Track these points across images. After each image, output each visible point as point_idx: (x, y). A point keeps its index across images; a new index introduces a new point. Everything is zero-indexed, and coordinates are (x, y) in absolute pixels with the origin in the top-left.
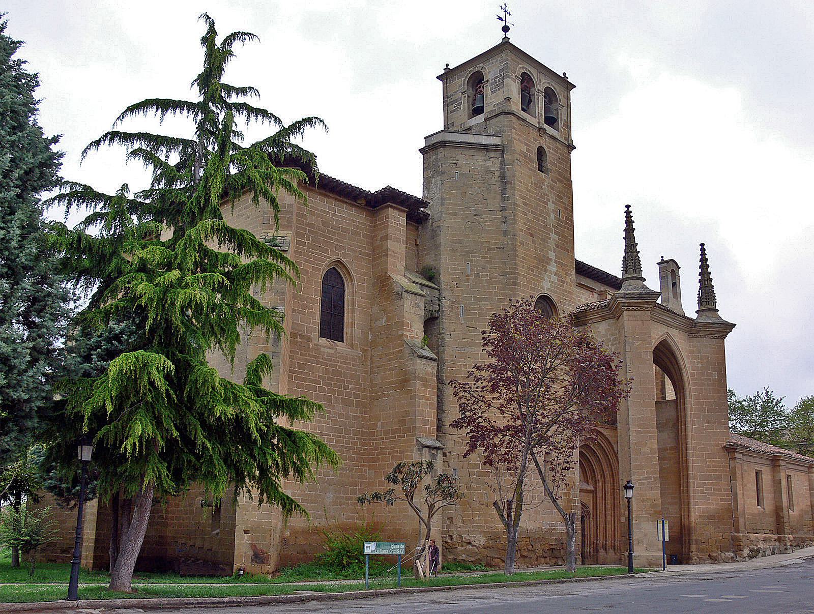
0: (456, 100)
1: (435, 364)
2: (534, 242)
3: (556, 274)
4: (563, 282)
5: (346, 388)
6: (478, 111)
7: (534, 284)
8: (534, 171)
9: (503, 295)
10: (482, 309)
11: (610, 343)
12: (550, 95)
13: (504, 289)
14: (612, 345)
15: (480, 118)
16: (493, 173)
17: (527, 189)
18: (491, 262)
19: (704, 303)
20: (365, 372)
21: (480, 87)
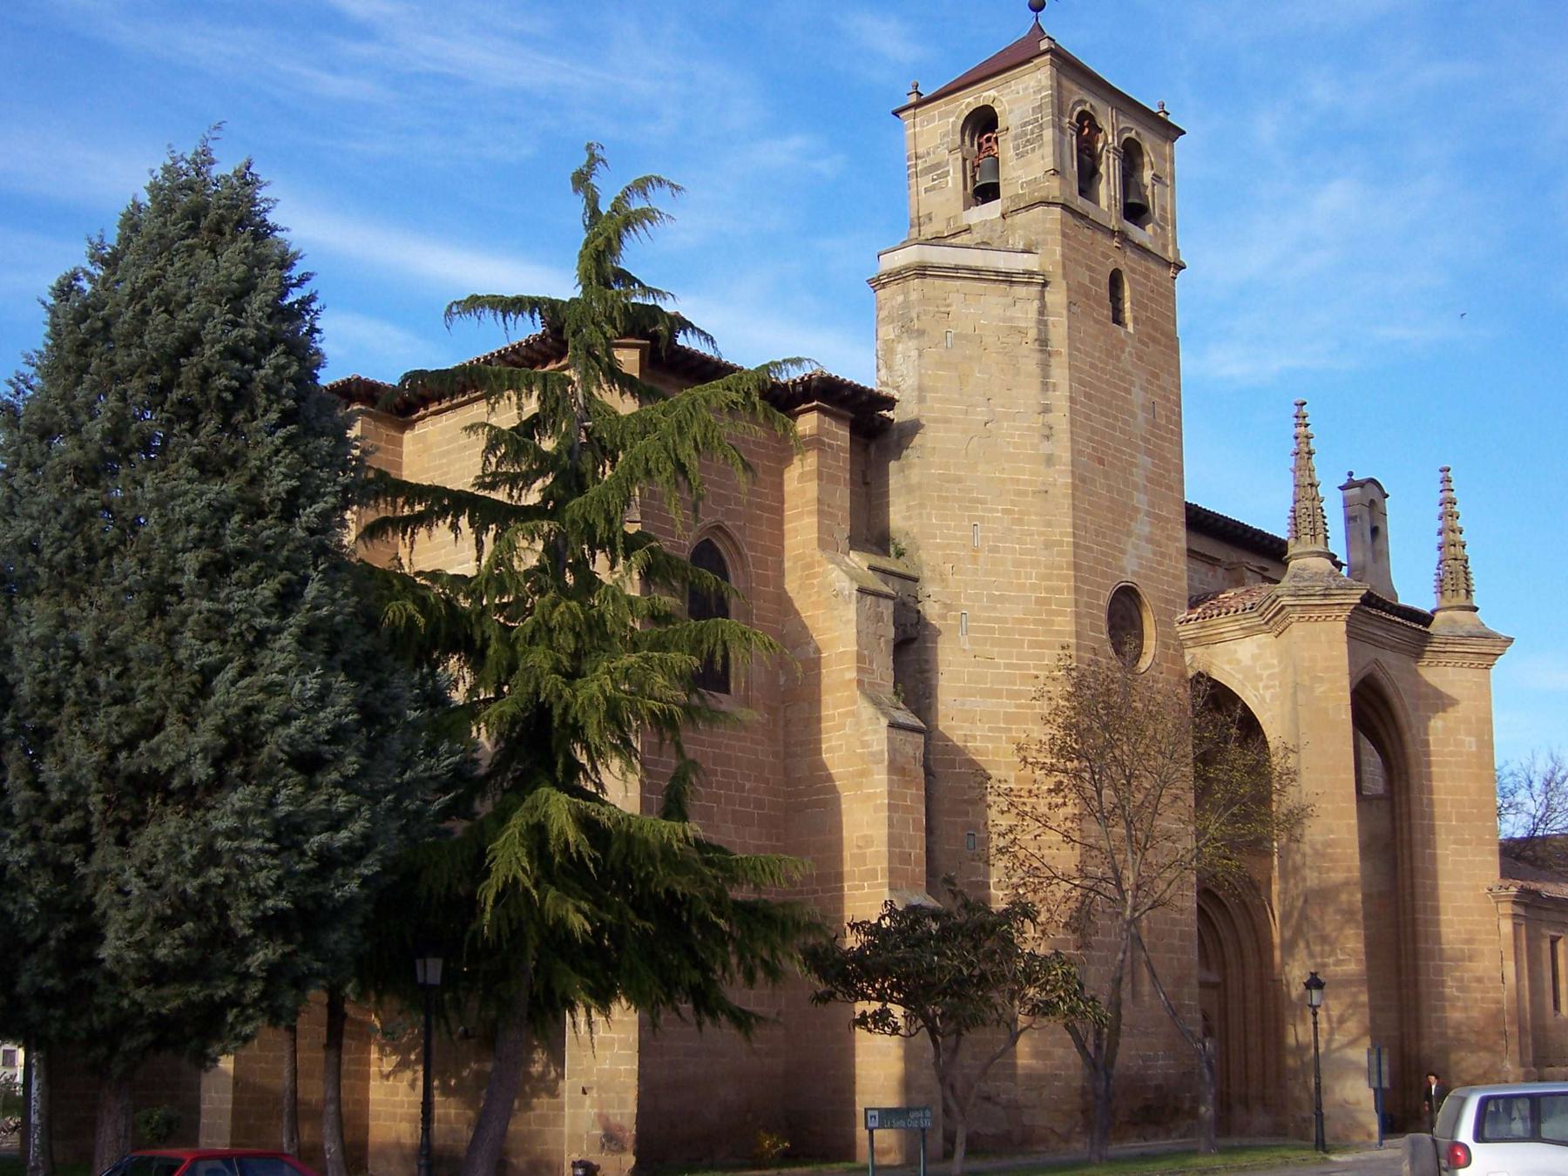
0: (936, 166)
1: (920, 739)
2: (1106, 475)
3: (1150, 540)
4: (1163, 555)
5: (741, 788)
6: (986, 193)
7: (1108, 565)
8: (1104, 325)
9: (1048, 589)
10: (1005, 620)
11: (1261, 685)
12: (1131, 154)
13: (1048, 577)
14: (1267, 687)
15: (993, 209)
16: (1021, 332)
17: (1093, 366)
18: (1020, 522)
19: (1449, 593)
20: (775, 754)
21: (988, 140)
